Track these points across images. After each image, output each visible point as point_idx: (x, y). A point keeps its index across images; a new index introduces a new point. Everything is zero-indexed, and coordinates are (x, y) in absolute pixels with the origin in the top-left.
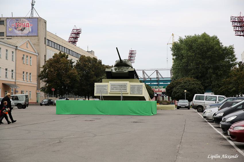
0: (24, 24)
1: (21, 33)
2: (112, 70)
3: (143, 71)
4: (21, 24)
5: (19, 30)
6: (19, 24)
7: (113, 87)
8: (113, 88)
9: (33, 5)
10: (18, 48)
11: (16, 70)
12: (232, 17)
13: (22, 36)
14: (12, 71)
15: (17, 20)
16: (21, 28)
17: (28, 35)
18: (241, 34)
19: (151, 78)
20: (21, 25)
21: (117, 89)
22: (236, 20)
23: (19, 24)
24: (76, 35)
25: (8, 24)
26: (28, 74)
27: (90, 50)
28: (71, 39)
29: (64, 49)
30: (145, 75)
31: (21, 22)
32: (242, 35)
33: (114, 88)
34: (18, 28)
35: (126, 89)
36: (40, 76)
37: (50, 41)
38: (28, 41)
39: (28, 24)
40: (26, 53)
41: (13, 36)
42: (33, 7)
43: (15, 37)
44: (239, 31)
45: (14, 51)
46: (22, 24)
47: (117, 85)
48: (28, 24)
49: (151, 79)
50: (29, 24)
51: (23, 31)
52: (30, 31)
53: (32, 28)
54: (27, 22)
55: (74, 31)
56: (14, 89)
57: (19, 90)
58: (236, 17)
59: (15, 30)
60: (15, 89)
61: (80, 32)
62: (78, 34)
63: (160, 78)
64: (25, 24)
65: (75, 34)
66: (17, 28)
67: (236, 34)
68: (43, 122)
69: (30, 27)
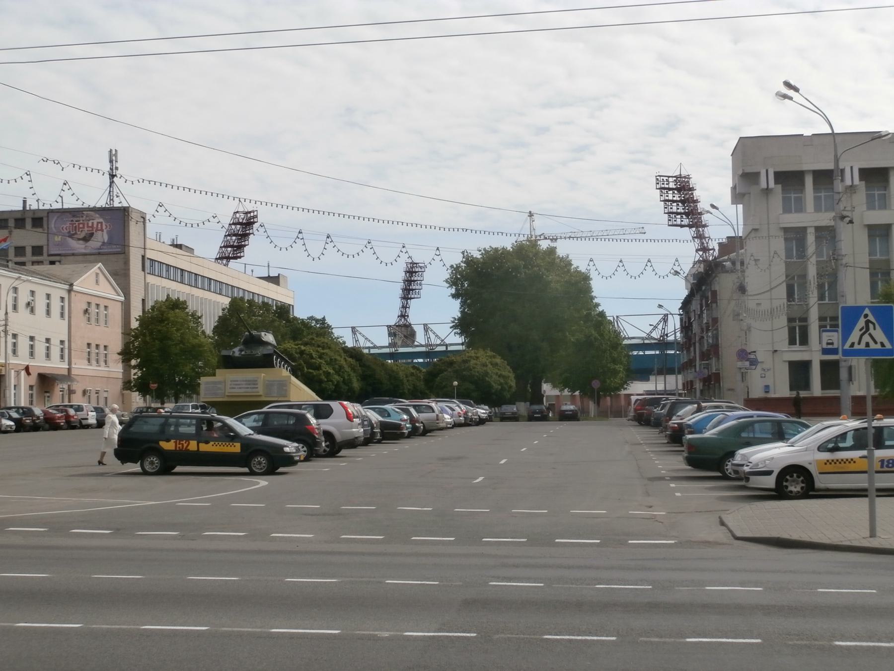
0: (90, 224)
1: (83, 246)
2: (234, 352)
3: (353, 328)
4: (84, 224)
6: (79, 224)
7: (234, 384)
8: (234, 386)
10: (74, 287)
11: (70, 341)
12: (659, 176)
13: (85, 255)
14: (62, 342)
15: (74, 216)
16: (82, 235)
18: (683, 223)
19: (447, 346)
20: (84, 228)
21: (240, 388)
22: (671, 184)
23: (79, 224)
25: (52, 225)
26: (102, 348)
27: (273, 274)
28: (229, 238)
29: (196, 280)
30: (432, 336)
31: (84, 218)
32: (686, 224)
33: (236, 386)
34: (76, 233)
35: (257, 388)
36: (126, 354)
38: (99, 268)
39: (101, 223)
40: (93, 297)
41: (66, 255)
43: (68, 257)
44: (678, 214)
45: (66, 296)
46: (86, 226)
47: (240, 381)
48: (100, 225)
49: (447, 348)
50: (104, 224)
52: (106, 241)
53: (109, 233)
54: (98, 219)
55: (238, 215)
56: (66, 386)
57: (78, 387)
58: (669, 177)
59: (70, 240)
60: (69, 386)
61: (256, 220)
63: (438, 345)
64: (93, 223)
66: (73, 234)
67: (670, 223)
69: (105, 231)
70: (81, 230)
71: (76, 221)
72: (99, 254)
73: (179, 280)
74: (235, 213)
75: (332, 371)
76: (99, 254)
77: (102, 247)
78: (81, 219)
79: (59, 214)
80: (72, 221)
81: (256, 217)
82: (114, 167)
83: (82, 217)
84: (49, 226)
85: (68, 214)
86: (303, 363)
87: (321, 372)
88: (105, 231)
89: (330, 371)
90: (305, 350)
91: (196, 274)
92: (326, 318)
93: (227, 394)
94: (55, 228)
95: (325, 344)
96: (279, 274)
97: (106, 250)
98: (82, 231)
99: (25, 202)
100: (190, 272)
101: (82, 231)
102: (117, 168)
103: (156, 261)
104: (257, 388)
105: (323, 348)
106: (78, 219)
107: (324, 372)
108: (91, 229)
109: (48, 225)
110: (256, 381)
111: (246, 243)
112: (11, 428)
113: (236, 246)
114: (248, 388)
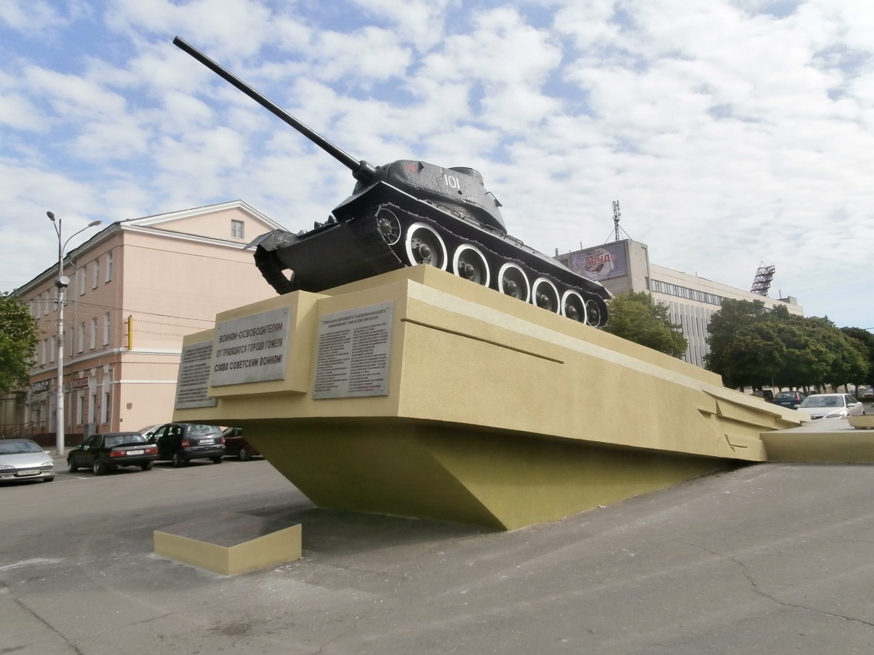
0: (600, 258)
5: (593, 271)
9: (617, 221)
15: (588, 254)
17: (609, 277)
20: (596, 261)
21: (238, 365)
23: (592, 259)
24: (765, 279)
28: (756, 285)
31: (595, 255)
35: (278, 359)
37: (680, 288)
39: (608, 255)
42: (618, 224)
48: (607, 257)
50: (610, 256)
51: (600, 270)
52: (613, 268)
54: (606, 253)
55: (761, 270)
61: (774, 271)
62: (770, 274)
64: (602, 257)
65: (763, 275)
66: (589, 268)
68: (725, 439)
69: (611, 261)
70: (594, 263)
71: (590, 257)
72: (609, 279)
73: (688, 297)
74: (759, 269)
75: (824, 350)
76: (609, 279)
77: (610, 274)
78: (594, 255)
79: (578, 255)
80: (588, 258)
81: (774, 269)
82: (617, 213)
83: (594, 254)
84: (572, 264)
85: (584, 253)
86: (780, 341)
87: (808, 350)
88: (611, 261)
89: (821, 349)
90: (784, 328)
91: (705, 293)
92: (828, 317)
93: (211, 393)
94: (576, 265)
95: (815, 323)
96: (789, 297)
97: (614, 276)
98: (595, 264)
99: (557, 251)
100: (699, 291)
101: (595, 264)
102: (620, 214)
103: (663, 282)
104: (278, 359)
105: (814, 327)
106: (591, 256)
107: (813, 351)
108: (601, 261)
109: (571, 264)
110: (279, 327)
111: (769, 286)
112: (16, 475)
113: (762, 289)
114: (255, 362)
